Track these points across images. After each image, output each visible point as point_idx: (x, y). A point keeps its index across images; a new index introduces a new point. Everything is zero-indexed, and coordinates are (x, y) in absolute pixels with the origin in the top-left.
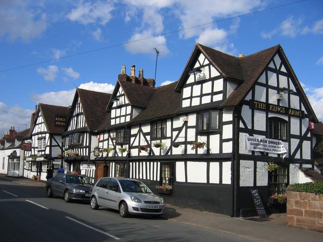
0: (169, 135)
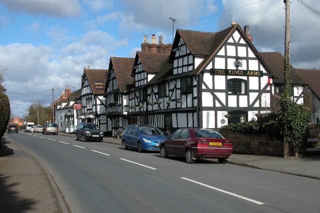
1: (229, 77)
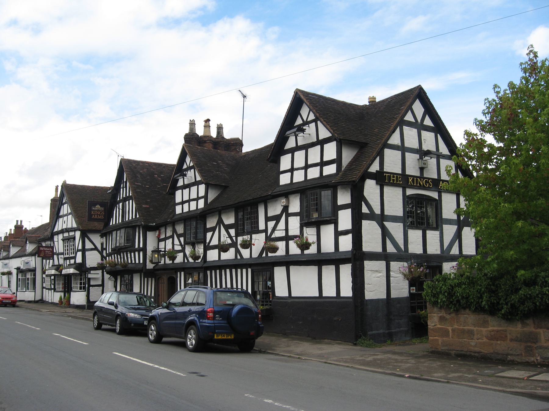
0: (262, 226)
1: (410, 192)
